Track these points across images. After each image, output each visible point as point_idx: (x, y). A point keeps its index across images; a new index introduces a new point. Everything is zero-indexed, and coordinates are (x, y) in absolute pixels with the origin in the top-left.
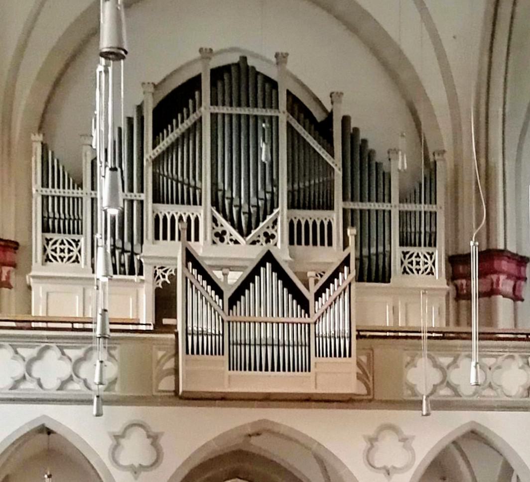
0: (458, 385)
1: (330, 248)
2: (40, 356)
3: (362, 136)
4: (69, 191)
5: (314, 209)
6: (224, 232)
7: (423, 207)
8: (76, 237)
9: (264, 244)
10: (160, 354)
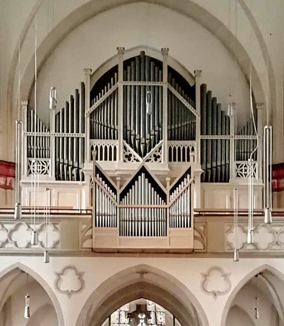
0: (258, 243)
1: (188, 162)
2: (16, 229)
3: (213, 96)
4: (40, 133)
5: (186, 140)
6: (131, 155)
7: (251, 137)
8: (46, 160)
9: (154, 161)
10: (84, 226)
